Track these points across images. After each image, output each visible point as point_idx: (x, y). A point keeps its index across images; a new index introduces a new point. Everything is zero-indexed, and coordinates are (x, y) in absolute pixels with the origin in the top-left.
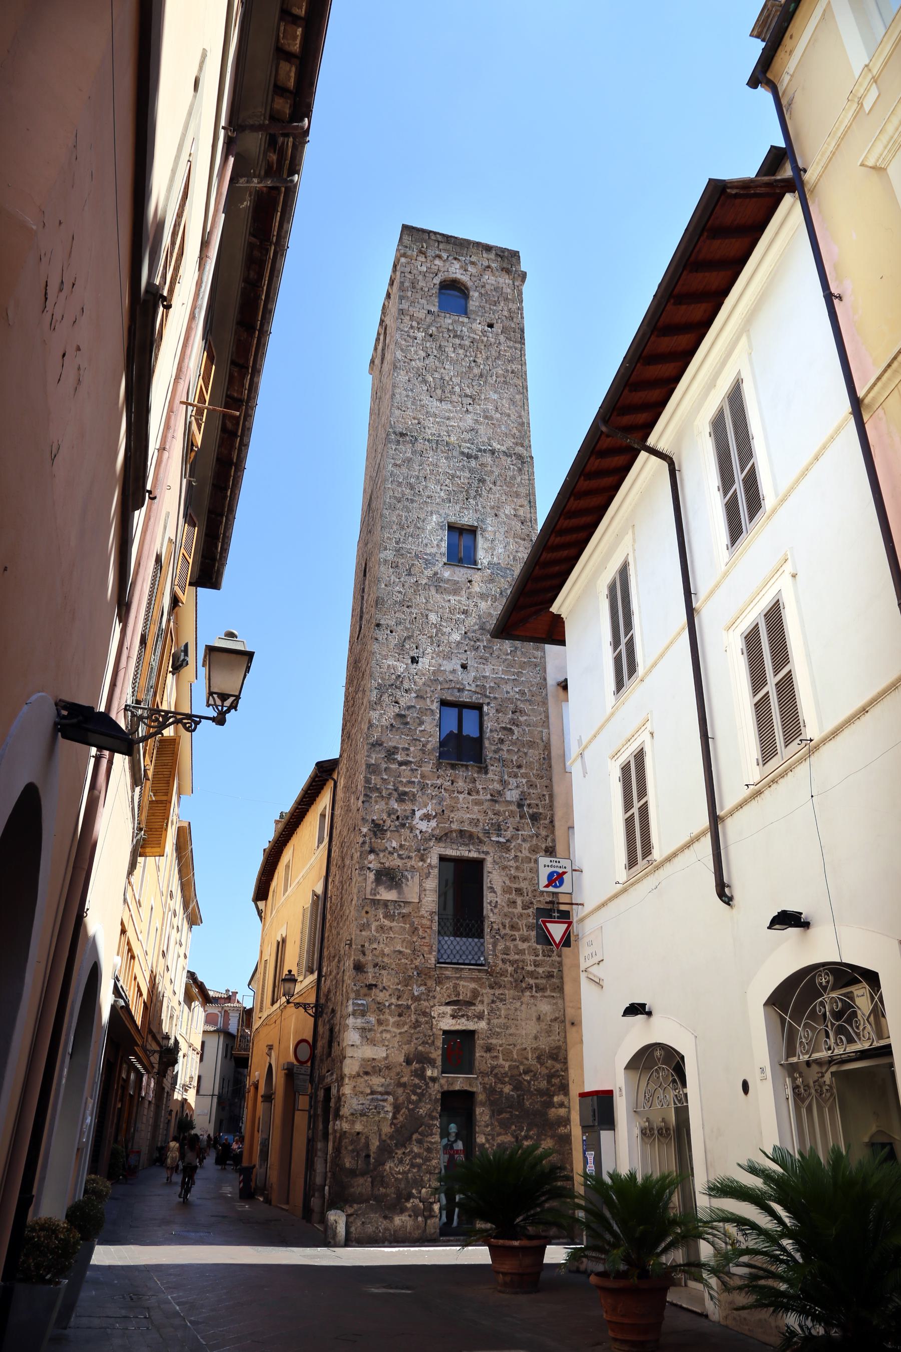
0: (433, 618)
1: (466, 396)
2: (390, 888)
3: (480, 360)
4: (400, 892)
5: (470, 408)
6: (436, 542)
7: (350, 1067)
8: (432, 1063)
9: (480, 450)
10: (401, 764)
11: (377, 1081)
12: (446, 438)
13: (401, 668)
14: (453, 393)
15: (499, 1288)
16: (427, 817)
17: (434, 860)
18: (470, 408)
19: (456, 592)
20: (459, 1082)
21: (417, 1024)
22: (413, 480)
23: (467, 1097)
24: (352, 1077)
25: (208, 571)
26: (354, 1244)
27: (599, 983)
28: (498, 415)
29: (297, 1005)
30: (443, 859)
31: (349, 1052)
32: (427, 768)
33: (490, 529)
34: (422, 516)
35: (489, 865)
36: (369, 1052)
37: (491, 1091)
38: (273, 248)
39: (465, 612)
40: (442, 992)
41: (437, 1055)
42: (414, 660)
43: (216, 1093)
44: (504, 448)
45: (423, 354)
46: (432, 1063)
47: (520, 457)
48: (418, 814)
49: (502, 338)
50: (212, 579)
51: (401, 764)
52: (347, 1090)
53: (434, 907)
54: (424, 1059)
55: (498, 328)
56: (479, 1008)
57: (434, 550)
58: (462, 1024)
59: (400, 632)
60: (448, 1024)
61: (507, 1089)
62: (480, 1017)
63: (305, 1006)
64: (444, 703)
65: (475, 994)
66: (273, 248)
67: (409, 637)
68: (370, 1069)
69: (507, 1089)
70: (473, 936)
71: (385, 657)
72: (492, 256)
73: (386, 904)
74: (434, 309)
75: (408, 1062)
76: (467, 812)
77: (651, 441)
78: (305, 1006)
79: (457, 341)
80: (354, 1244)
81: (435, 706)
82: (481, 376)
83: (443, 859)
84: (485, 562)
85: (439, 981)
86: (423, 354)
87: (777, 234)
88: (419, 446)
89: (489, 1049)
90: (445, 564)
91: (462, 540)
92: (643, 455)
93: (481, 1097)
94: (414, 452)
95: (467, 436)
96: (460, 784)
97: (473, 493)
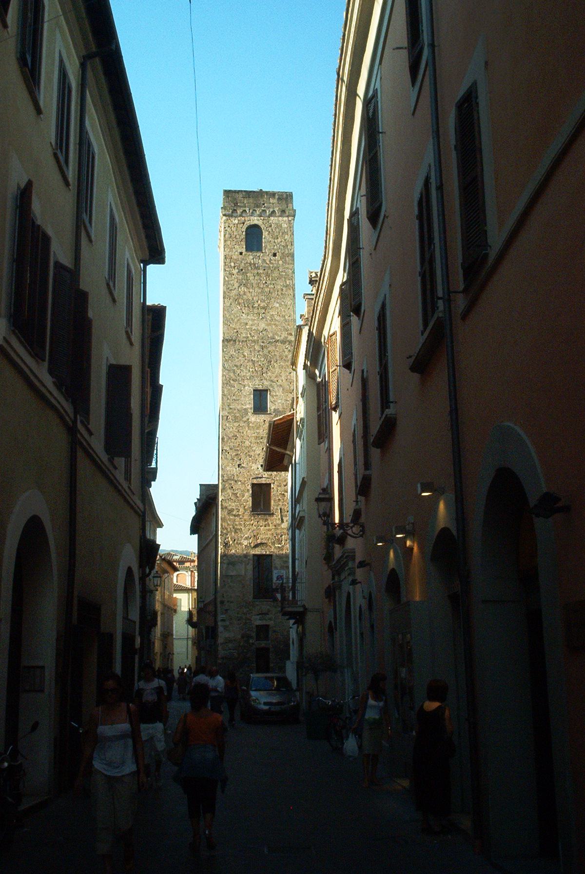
7: (220, 640)
11: (230, 645)
20: (263, 644)
21: (246, 623)
23: (266, 650)
24: (222, 644)
26: (114, 47)
31: (220, 635)
32: (248, 513)
36: (227, 635)
38: (137, 657)
41: (254, 634)
46: (251, 637)
52: (220, 648)
53: (251, 576)
54: (249, 637)
56: (270, 616)
60: (259, 623)
62: (270, 619)
65: (269, 611)
66: (137, 657)
68: (228, 641)
74: (244, 250)
75: (243, 637)
80: (114, 47)
81: (249, 487)
87: (22, 360)
97: (265, 370)
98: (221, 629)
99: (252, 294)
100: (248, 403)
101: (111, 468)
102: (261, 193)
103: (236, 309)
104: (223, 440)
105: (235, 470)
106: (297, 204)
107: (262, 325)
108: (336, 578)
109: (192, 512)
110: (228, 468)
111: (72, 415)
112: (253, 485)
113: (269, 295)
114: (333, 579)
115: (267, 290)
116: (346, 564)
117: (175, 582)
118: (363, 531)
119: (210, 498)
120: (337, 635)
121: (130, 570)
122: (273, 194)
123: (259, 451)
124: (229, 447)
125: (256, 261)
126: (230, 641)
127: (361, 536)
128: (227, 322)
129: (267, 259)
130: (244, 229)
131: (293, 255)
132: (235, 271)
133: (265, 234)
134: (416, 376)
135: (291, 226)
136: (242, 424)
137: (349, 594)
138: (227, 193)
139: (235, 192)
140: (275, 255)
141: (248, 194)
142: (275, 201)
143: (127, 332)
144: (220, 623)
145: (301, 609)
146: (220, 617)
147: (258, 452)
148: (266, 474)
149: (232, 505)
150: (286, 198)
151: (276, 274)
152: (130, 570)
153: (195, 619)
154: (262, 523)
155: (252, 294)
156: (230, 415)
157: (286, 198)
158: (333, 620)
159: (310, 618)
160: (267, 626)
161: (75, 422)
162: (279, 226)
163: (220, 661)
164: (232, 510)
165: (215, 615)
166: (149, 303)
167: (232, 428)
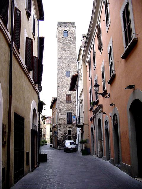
0: (65, 84)
7: (59, 134)
11: (61, 135)
15: (52, 177)
17: (66, 113)
19: (67, 81)
27: (44, 109)
30: (67, 113)
32: (65, 103)
36: (60, 133)
37: (73, 136)
41: (67, 133)
42: (63, 90)
43: (50, 134)
50: (41, 85)
58: (70, 130)
62: (72, 129)
64: (66, 95)
70: (67, 121)
72: (100, 153)
76: (69, 108)
79: (66, 42)
81: (66, 96)
83: (67, 113)
98: (59, 131)
99: (65, 47)
100: (65, 74)
101: (28, 73)
102: (67, 23)
103: (62, 51)
104: (58, 83)
105: (62, 91)
106: (76, 25)
107: (68, 55)
108: (94, 115)
109: (51, 104)
110: (60, 91)
111: (11, 40)
113: (70, 48)
115: (69, 46)
116: (99, 109)
117: (40, 153)
118: (109, 96)
119: (55, 99)
120: (95, 131)
121: (34, 109)
122: (70, 23)
123: (68, 87)
124: (60, 86)
126: (61, 135)
127: (109, 97)
128: (59, 54)
129: (69, 38)
131: (75, 37)
132: (61, 42)
135: (75, 30)
136: (63, 80)
137: (99, 119)
138: (58, 22)
140: (71, 37)
141: (64, 23)
143: (33, 34)
144: (58, 130)
145: (83, 125)
146: (59, 128)
148: (69, 92)
149: (61, 100)
150: (74, 24)
151: (71, 42)
152: (34, 109)
153: (51, 130)
154: (69, 104)
155: (65, 47)
156: (60, 77)
157: (74, 24)
159: (85, 127)
160: (71, 131)
161: (12, 43)
163: (59, 140)
164: (61, 102)
165: (57, 128)
167: (61, 81)
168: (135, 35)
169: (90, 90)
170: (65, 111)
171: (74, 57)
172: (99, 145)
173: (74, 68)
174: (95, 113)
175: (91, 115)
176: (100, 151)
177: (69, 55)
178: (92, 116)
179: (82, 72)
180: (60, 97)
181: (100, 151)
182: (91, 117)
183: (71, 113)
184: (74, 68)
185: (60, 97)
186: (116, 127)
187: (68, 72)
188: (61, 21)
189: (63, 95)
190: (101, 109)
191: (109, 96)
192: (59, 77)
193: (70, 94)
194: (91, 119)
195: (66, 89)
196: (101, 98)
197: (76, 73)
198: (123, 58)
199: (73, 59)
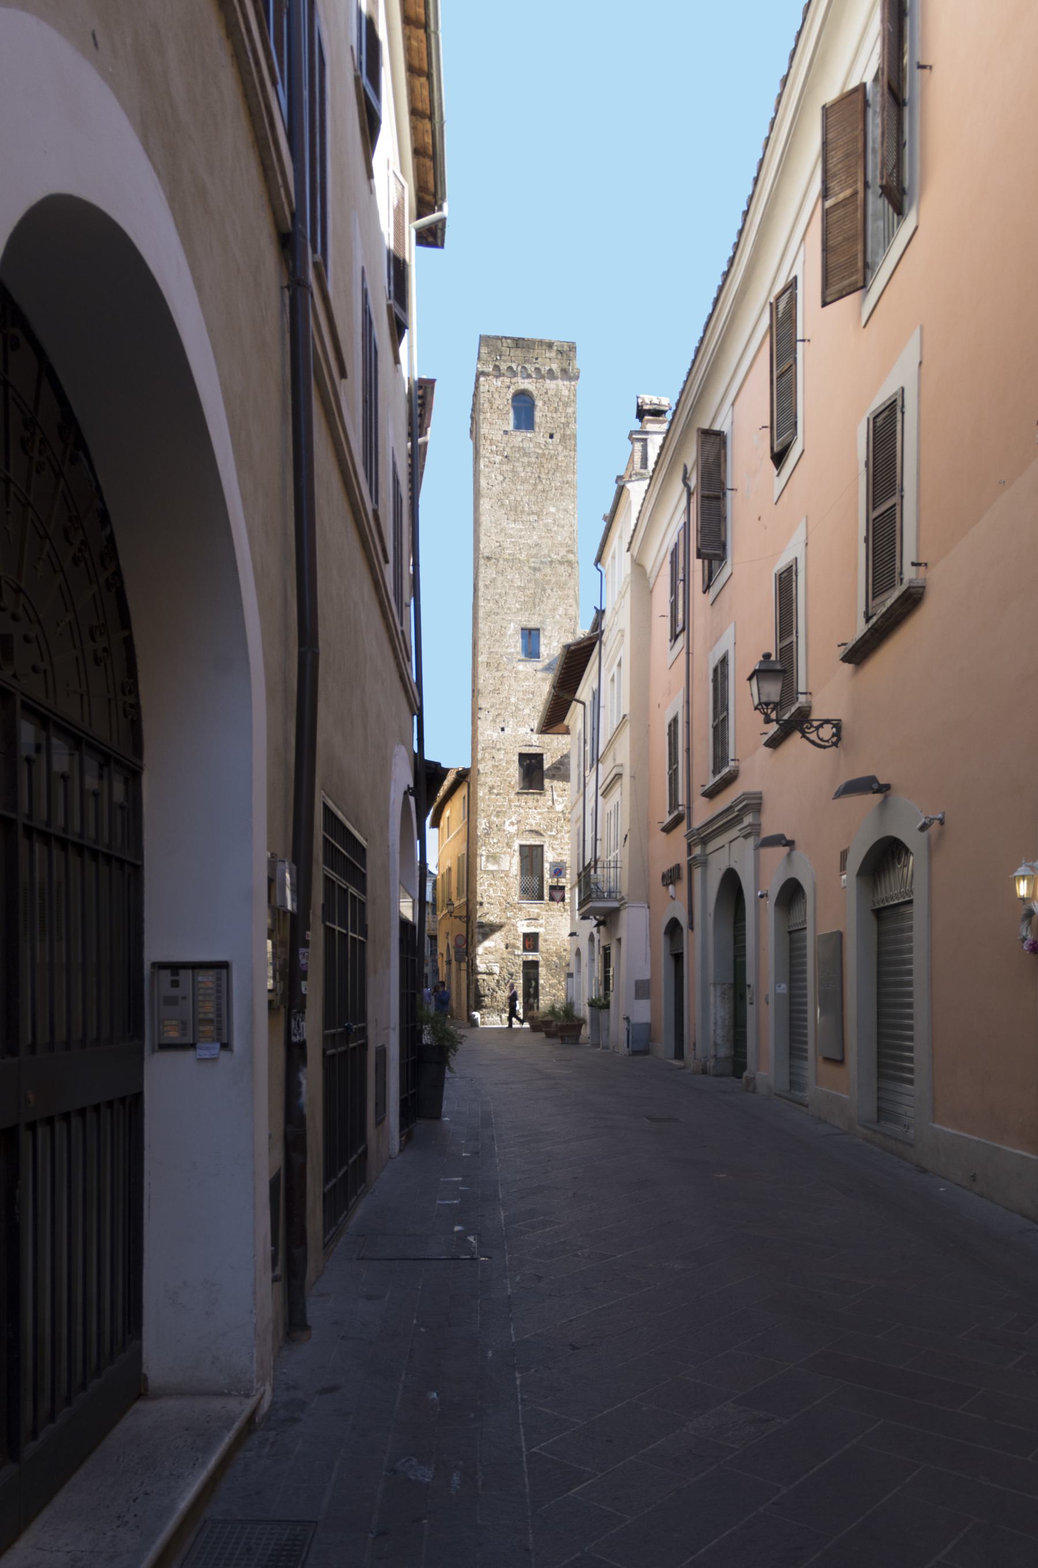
0: (513, 700)
1: (533, 513)
2: (494, 864)
3: (543, 476)
4: (499, 866)
5: (535, 525)
6: (515, 644)
8: (518, 948)
9: (542, 562)
10: (498, 794)
12: (518, 556)
13: (495, 735)
14: (522, 512)
16: (512, 824)
17: (516, 847)
18: (535, 525)
20: (531, 956)
22: (497, 597)
25: (673, 928)
28: (555, 528)
29: (456, 917)
30: (521, 846)
33: (549, 628)
34: (504, 625)
35: (545, 848)
39: (533, 693)
40: (522, 915)
42: (503, 729)
44: (559, 558)
45: (500, 478)
46: (518, 948)
47: (570, 563)
48: (507, 823)
49: (560, 448)
51: (498, 794)
55: (557, 437)
56: (541, 921)
57: (513, 650)
59: (494, 712)
61: (555, 959)
62: (541, 926)
63: (460, 918)
65: (539, 915)
67: (499, 715)
69: (555, 959)
71: (485, 730)
73: (492, 872)
76: (535, 819)
77: (578, 696)
78: (460, 918)
79: (526, 460)
82: (544, 491)
83: (521, 846)
84: (545, 654)
85: (520, 909)
86: (500, 478)
88: (500, 567)
89: (546, 941)
90: (518, 793)
91: (531, 637)
92: (574, 703)
93: (541, 963)
94: (497, 573)
95: (534, 551)
96: (530, 804)
97: (537, 600)
106: (580, 362)
108: (697, 851)
112: (521, 755)
114: (690, 852)
118: (838, 735)
122: (550, 345)
125: (526, 444)
127: (835, 744)
130: (509, 396)
133: (539, 403)
134: (848, 667)
137: (731, 882)
138: (485, 340)
139: (497, 338)
140: (551, 436)
142: (553, 354)
147: (499, 384)
148: (535, 738)
150: (567, 352)
157: (567, 352)
158: (699, 599)
162: (558, 393)
164: (492, 788)
166: (426, 758)
168: (914, 568)
169: (668, 719)
170: (511, 837)
171: (563, 552)
172: (719, 1011)
173: (561, 611)
174: (704, 841)
175: (672, 850)
176: (719, 1041)
177: (540, 537)
178: (683, 860)
179: (619, 625)
180: (490, 763)
181: (719, 1041)
182: (671, 865)
183: (542, 846)
184: (561, 611)
185: (490, 763)
186: (886, 919)
187: (531, 637)
188: (500, 334)
189: (501, 755)
190: (748, 820)
191: (838, 735)
192: (570, 410)
193: (538, 751)
194: (671, 877)
195: (519, 724)
196: (758, 767)
197: (583, 630)
198: (847, 658)
199: (561, 563)
